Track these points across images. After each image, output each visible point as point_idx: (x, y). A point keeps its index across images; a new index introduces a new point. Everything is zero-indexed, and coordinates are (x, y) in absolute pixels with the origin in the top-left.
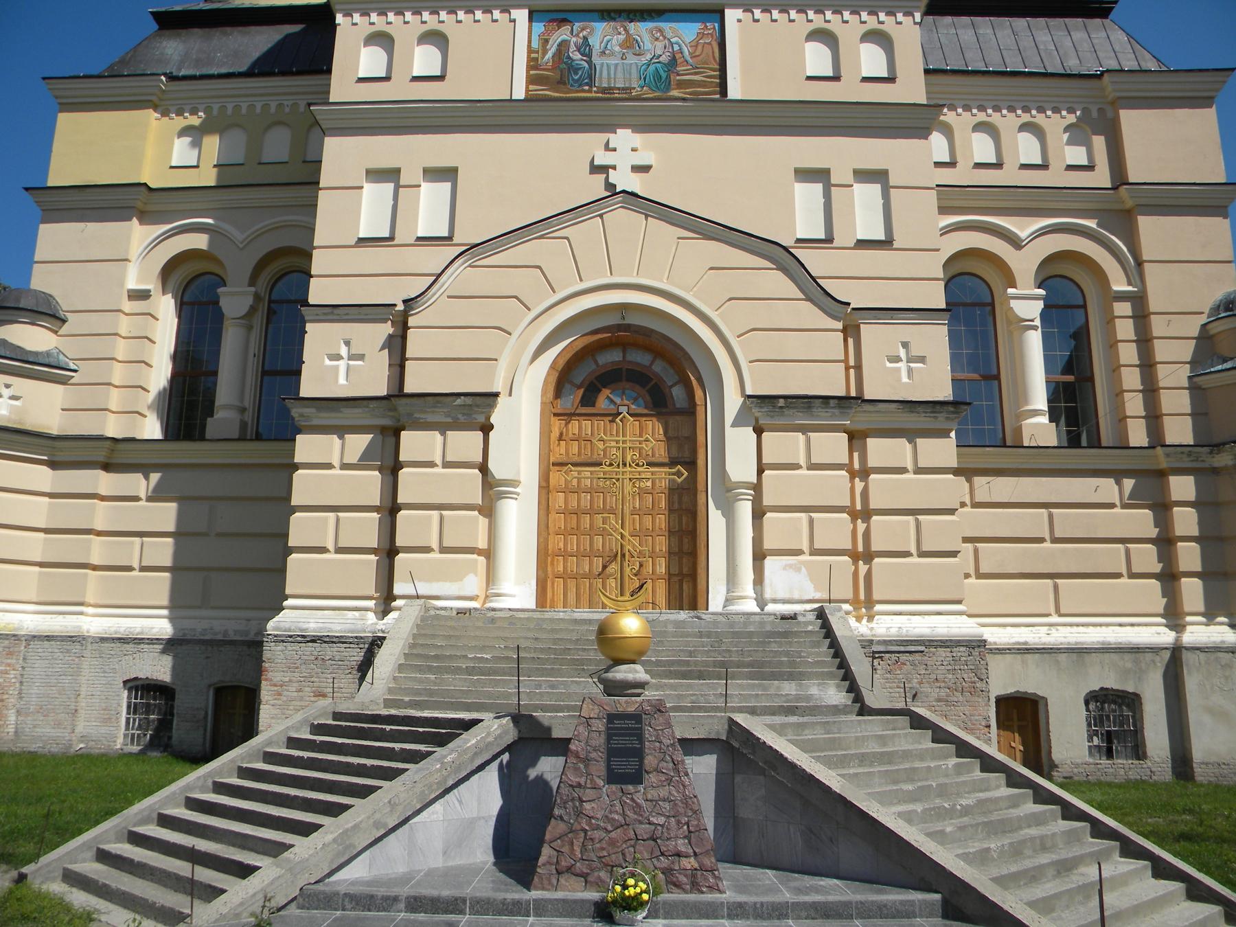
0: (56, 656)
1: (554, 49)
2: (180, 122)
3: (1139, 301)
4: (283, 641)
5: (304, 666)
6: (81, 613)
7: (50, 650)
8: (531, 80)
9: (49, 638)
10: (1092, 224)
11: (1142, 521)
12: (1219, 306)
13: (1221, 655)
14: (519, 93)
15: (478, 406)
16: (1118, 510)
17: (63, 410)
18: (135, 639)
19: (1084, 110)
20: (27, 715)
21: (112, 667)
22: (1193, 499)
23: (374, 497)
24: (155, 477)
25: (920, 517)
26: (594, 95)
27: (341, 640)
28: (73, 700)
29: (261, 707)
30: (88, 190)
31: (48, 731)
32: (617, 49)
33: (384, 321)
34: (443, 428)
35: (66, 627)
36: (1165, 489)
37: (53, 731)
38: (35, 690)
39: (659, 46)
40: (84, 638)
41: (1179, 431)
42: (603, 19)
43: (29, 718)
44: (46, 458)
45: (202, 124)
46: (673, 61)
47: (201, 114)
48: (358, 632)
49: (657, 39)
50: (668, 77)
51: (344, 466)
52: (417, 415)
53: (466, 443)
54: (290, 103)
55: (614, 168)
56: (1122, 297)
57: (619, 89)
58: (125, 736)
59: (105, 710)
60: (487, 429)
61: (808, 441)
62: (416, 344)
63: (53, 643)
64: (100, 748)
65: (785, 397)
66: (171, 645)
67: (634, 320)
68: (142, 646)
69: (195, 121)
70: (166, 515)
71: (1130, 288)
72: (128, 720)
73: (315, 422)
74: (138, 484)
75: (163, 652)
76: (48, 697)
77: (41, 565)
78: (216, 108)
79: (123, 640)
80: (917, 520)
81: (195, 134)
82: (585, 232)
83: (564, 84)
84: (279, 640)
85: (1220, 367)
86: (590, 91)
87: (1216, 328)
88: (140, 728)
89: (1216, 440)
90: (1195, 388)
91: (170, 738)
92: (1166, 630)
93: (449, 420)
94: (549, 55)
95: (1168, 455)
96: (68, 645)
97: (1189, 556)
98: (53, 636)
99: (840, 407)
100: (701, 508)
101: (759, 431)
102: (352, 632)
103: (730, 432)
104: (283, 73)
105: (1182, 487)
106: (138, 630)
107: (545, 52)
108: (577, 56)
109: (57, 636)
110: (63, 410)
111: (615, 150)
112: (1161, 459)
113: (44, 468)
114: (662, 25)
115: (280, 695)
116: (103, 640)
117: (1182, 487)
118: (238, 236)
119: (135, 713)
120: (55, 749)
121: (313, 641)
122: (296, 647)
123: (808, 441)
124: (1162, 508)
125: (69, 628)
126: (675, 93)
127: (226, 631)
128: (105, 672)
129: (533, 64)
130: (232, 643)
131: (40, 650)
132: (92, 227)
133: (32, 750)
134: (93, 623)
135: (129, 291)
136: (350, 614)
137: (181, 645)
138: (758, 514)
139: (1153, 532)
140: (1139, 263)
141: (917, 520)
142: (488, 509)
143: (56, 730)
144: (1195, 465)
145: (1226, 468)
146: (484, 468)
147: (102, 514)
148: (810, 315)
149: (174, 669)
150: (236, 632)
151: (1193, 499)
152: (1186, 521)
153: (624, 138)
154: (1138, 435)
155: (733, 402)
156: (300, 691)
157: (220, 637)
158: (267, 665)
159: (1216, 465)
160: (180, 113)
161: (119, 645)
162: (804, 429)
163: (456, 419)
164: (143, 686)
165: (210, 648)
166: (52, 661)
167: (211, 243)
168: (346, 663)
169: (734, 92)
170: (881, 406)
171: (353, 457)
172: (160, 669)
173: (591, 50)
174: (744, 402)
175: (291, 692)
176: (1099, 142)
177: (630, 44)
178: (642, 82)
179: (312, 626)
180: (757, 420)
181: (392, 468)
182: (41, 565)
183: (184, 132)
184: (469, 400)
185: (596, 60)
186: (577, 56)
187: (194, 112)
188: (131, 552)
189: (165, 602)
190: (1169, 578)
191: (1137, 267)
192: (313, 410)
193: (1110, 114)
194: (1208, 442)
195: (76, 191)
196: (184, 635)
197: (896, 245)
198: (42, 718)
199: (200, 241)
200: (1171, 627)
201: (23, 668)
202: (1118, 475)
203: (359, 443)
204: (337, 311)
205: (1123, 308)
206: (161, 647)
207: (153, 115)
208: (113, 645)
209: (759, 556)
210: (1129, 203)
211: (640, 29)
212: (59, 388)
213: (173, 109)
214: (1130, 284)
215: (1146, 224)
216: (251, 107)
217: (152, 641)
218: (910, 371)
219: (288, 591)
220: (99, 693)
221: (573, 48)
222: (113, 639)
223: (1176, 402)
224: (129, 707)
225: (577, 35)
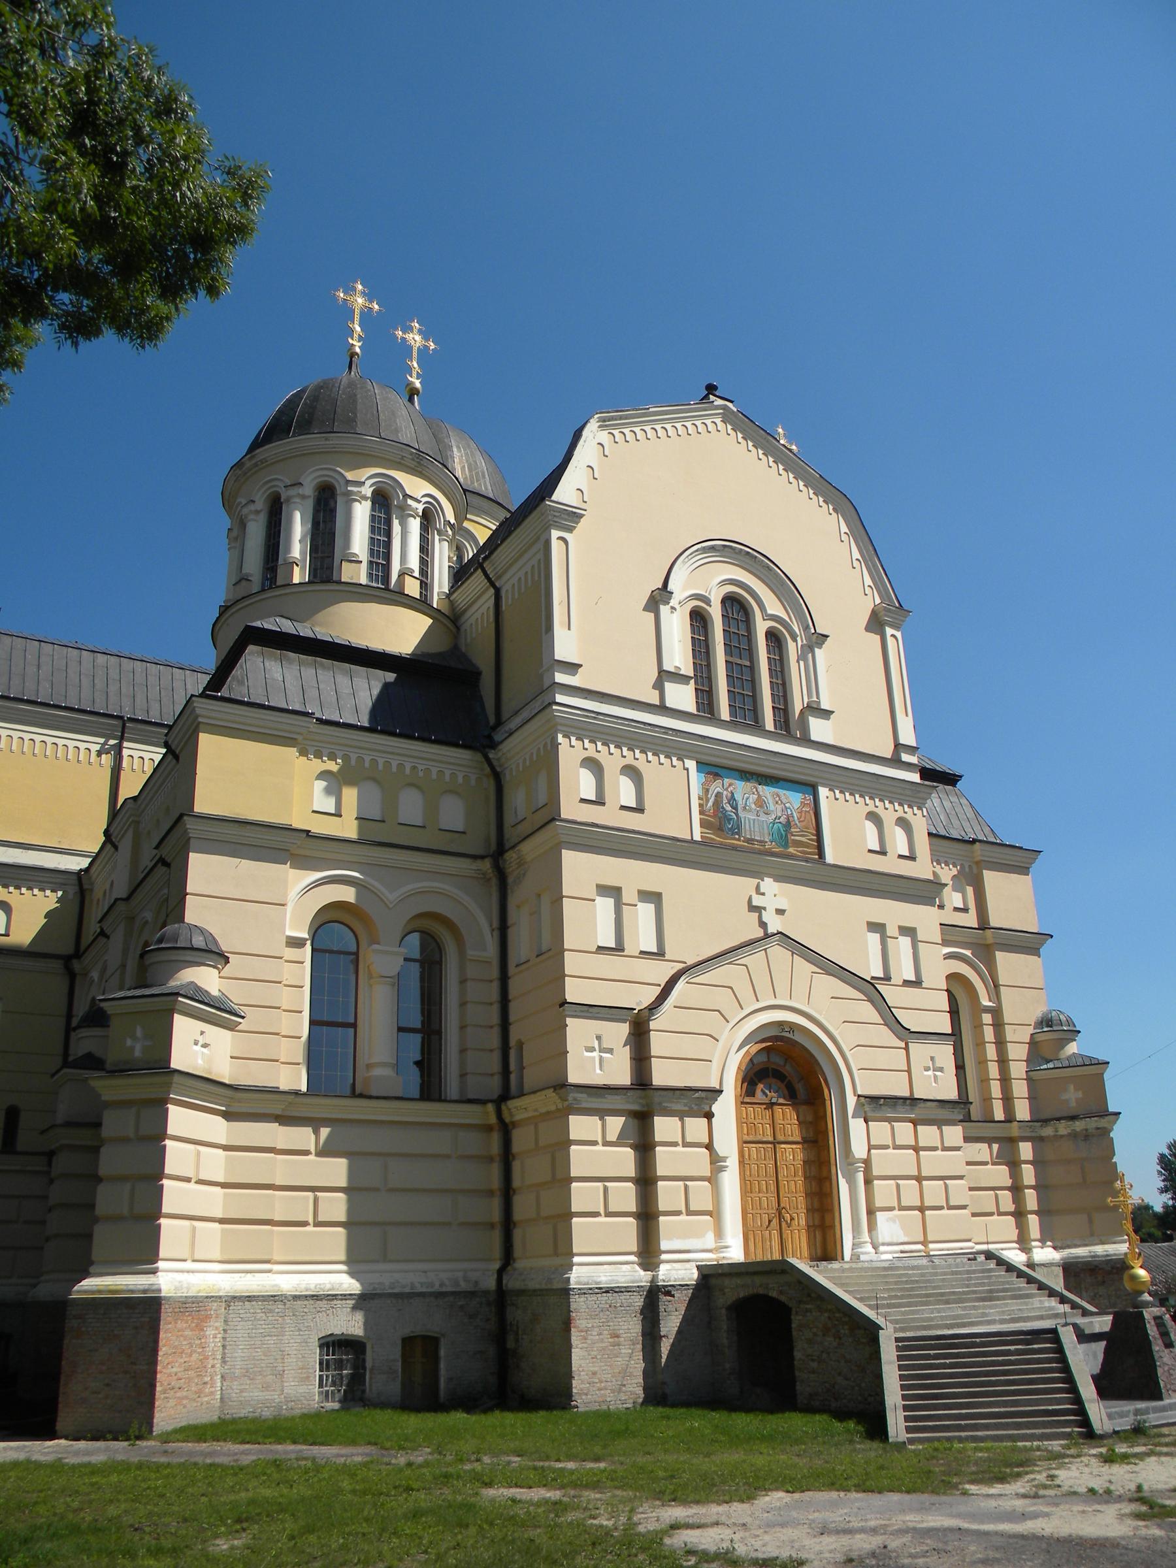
0: (259, 1316)
1: (713, 798)
2: (319, 765)
3: (997, 1012)
4: (585, 1294)
5: (601, 1314)
6: (269, 1271)
7: (252, 1311)
8: (703, 824)
9: (250, 1298)
10: (968, 953)
11: (1001, 1175)
12: (1042, 1022)
13: (1053, 1268)
14: (697, 837)
15: (707, 1099)
16: (989, 1166)
17: (231, 1057)
18: (328, 1295)
19: (962, 866)
20: (234, 1378)
21: (306, 1324)
22: (1031, 1159)
23: (630, 1170)
24: (325, 1132)
25: (947, 1182)
26: (742, 843)
27: (627, 1290)
28: (280, 1361)
29: (573, 1350)
30: (248, 827)
31: (256, 1394)
32: (753, 806)
33: (624, 1021)
34: (682, 1116)
35: (263, 1286)
36: (1016, 1151)
37: (261, 1394)
38: (239, 1353)
39: (779, 807)
40: (285, 1296)
41: (1023, 1111)
42: (742, 779)
43: (235, 1383)
44: (224, 1108)
45: (340, 770)
46: (788, 825)
47: (339, 761)
48: (637, 1282)
49: (777, 803)
50: (786, 835)
51: (606, 1143)
52: (665, 1104)
53: (696, 1127)
54: (423, 767)
55: (765, 909)
56: (987, 1010)
57: (757, 841)
58: (320, 1393)
59: (302, 1369)
60: (709, 1116)
61: (893, 1128)
62: (658, 1044)
63: (254, 1303)
64: (302, 1408)
65: (885, 1098)
66: (362, 1301)
67: (797, 1037)
68: (335, 1302)
69: (333, 766)
70: (337, 1170)
71: (991, 1004)
72: (321, 1377)
73: (584, 1105)
74: (303, 1137)
75: (355, 1308)
76: (254, 1359)
77: (222, 1221)
78: (353, 757)
79: (316, 1297)
80: (945, 1183)
81: (335, 783)
82: (755, 960)
83: (722, 830)
84: (583, 1292)
85: (1045, 1066)
86: (739, 840)
87: (1039, 1038)
88: (334, 1384)
89: (1043, 1117)
90: (1029, 1080)
91: (364, 1391)
92: (1019, 1252)
93: (686, 1108)
94: (710, 803)
95: (1020, 1128)
96: (270, 1305)
97: (1031, 1199)
98: (254, 1296)
99: (911, 1105)
100: (834, 1177)
101: (866, 1121)
102: (633, 1282)
103: (851, 1121)
104: (422, 739)
105: (1026, 1150)
106: (328, 1286)
107: (708, 801)
108: (728, 808)
109: (258, 1296)
110: (231, 1057)
111: (763, 894)
112: (1014, 1130)
113: (219, 1119)
114: (781, 792)
115: (586, 1339)
116: (296, 1298)
117: (1026, 1150)
118: (391, 897)
119: (328, 1369)
120: (267, 1414)
121: (607, 1292)
122: (594, 1298)
123: (893, 1128)
124: (1014, 1165)
125: (268, 1288)
126: (791, 850)
127: (412, 1284)
128: (300, 1330)
129: (701, 812)
130: (422, 1295)
131: (241, 1311)
132: (247, 865)
133: (242, 1415)
134: (287, 1281)
135: (289, 937)
136: (625, 1267)
137: (373, 1299)
138: (868, 1182)
139: (1009, 1183)
140: (996, 986)
141: (945, 1183)
142: (713, 1180)
143: (264, 1394)
144: (1033, 1134)
145: (1048, 1137)
146: (709, 1146)
147: (281, 1169)
148: (886, 1036)
149: (366, 1324)
150: (422, 1284)
151: (1031, 1159)
152: (1028, 1174)
153: (768, 884)
154: (999, 1115)
155: (851, 1101)
156: (600, 1334)
157: (407, 1290)
158: (574, 1315)
159: (1043, 1134)
160: (319, 755)
161: (312, 1302)
162: (889, 1120)
163: (691, 1108)
164: (334, 1343)
165: (400, 1301)
166: (255, 1323)
167: (358, 895)
168: (632, 1308)
169: (830, 858)
170: (929, 1104)
171: (612, 1136)
172: (352, 1325)
173: (737, 804)
174: (858, 1100)
175: (594, 1336)
176: (970, 890)
177: (760, 803)
178: (771, 837)
179: (603, 1279)
180: (865, 1112)
181: (645, 1148)
182: (222, 1221)
183: (323, 775)
184: (703, 1094)
185: (741, 814)
186: (728, 808)
187: (332, 757)
188: (301, 1206)
189: (343, 1257)
190: (1019, 1214)
191: (995, 988)
192: (584, 1095)
193: (975, 871)
194: (1039, 1119)
195: (237, 825)
196: (375, 1289)
197: (924, 985)
198: (248, 1382)
199: (348, 894)
200: (1022, 1250)
201: (225, 1331)
202: (989, 1141)
203: (616, 1124)
204: (591, 1010)
205: (987, 1018)
206: (353, 1302)
207: (293, 752)
208: (306, 1302)
209: (871, 1212)
210: (990, 941)
211: (767, 791)
212: (227, 1034)
213: (312, 750)
214: (990, 1001)
215: (1000, 956)
216: (388, 764)
217: (344, 1297)
218: (935, 1077)
219: (575, 1251)
220: (295, 1352)
221: (725, 801)
222: (306, 1296)
223: (1020, 1089)
224: (321, 1363)
225: (727, 789)
